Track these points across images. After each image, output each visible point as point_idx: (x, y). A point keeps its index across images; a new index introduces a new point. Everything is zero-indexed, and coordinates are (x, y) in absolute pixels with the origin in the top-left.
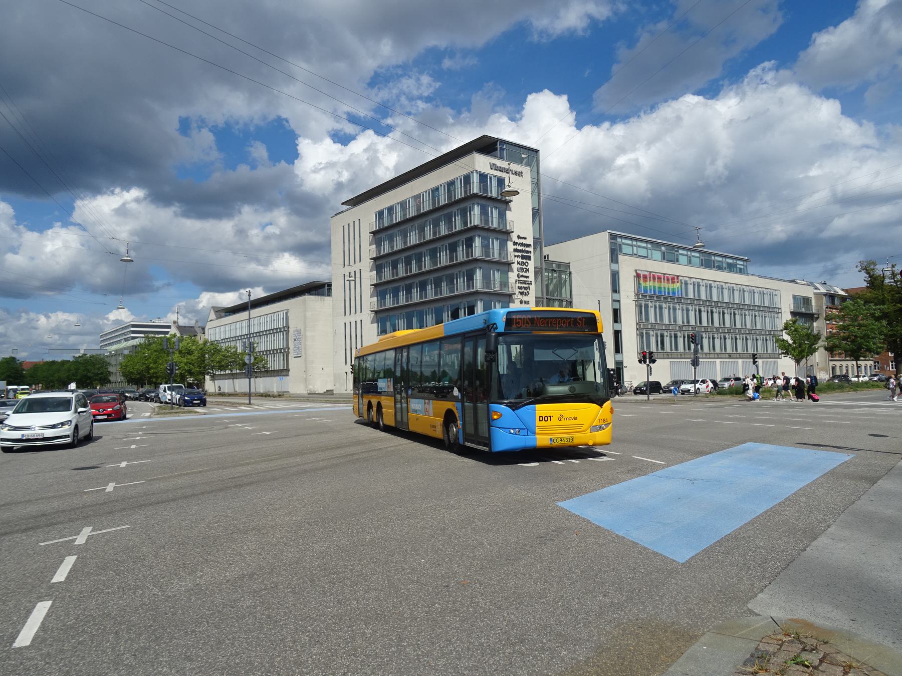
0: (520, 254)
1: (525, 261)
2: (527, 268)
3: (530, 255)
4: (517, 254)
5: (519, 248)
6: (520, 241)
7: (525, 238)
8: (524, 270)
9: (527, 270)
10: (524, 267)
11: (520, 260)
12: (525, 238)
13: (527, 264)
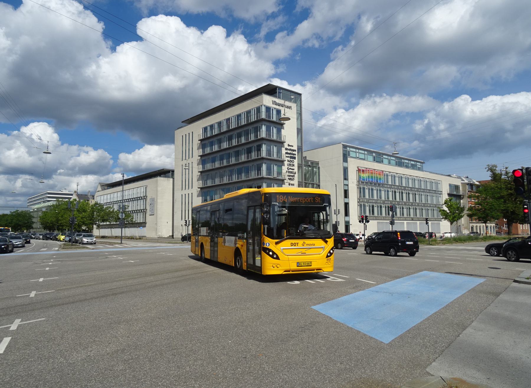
0: (289, 156)
1: (292, 160)
2: (293, 164)
3: (295, 156)
4: (287, 155)
5: (289, 152)
6: (289, 148)
7: (292, 146)
8: (292, 165)
9: (293, 165)
10: (292, 163)
11: (289, 159)
12: (292, 146)
13: (293, 162)
